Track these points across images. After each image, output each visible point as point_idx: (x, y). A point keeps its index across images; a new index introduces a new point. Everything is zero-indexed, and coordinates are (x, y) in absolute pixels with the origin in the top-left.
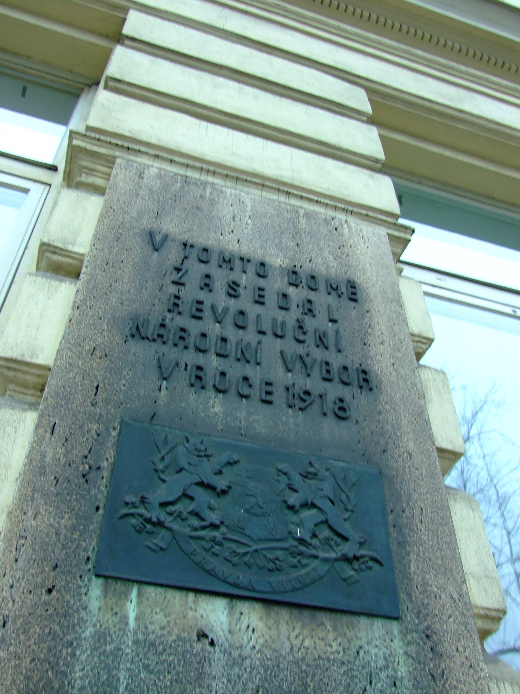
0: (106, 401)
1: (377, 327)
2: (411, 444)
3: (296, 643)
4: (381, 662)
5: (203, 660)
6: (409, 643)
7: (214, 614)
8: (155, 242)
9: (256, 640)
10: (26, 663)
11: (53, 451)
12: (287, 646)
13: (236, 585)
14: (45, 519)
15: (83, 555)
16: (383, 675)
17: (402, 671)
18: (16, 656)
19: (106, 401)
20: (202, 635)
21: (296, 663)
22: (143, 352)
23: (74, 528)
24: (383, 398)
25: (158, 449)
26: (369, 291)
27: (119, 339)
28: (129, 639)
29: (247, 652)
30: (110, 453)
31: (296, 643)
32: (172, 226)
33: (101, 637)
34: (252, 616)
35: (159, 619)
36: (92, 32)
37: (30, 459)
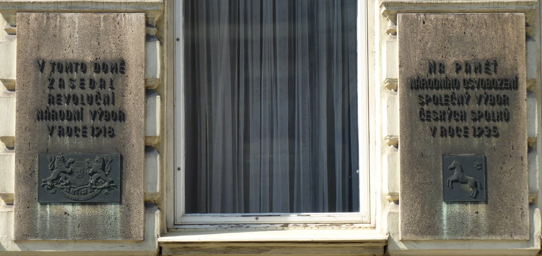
0: (33, 148)
1: (130, 85)
2: (134, 140)
3: (90, 212)
4: (113, 214)
5: (66, 219)
6: (122, 208)
7: (69, 208)
8: (41, 65)
9: (80, 213)
10: (26, 224)
11: (21, 169)
12: (87, 213)
13: (74, 200)
14: (24, 189)
15: (34, 197)
16: (113, 217)
17: (118, 216)
18: (24, 223)
19: (33, 148)
20: (66, 213)
21: (90, 217)
22: (43, 124)
23: (31, 191)
24: (127, 122)
25: (219, 20)
26: (129, 63)
27: (33, 121)
28: (48, 216)
29: (77, 216)
30: (37, 166)
31: (90, 212)
32: (45, 54)
33: (42, 217)
34: (78, 208)
35: (55, 211)
36: (244, 247)
37: (16, 173)
